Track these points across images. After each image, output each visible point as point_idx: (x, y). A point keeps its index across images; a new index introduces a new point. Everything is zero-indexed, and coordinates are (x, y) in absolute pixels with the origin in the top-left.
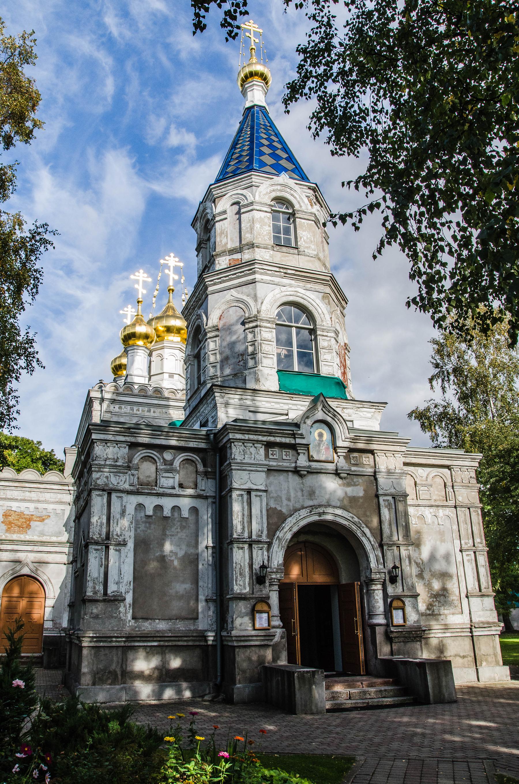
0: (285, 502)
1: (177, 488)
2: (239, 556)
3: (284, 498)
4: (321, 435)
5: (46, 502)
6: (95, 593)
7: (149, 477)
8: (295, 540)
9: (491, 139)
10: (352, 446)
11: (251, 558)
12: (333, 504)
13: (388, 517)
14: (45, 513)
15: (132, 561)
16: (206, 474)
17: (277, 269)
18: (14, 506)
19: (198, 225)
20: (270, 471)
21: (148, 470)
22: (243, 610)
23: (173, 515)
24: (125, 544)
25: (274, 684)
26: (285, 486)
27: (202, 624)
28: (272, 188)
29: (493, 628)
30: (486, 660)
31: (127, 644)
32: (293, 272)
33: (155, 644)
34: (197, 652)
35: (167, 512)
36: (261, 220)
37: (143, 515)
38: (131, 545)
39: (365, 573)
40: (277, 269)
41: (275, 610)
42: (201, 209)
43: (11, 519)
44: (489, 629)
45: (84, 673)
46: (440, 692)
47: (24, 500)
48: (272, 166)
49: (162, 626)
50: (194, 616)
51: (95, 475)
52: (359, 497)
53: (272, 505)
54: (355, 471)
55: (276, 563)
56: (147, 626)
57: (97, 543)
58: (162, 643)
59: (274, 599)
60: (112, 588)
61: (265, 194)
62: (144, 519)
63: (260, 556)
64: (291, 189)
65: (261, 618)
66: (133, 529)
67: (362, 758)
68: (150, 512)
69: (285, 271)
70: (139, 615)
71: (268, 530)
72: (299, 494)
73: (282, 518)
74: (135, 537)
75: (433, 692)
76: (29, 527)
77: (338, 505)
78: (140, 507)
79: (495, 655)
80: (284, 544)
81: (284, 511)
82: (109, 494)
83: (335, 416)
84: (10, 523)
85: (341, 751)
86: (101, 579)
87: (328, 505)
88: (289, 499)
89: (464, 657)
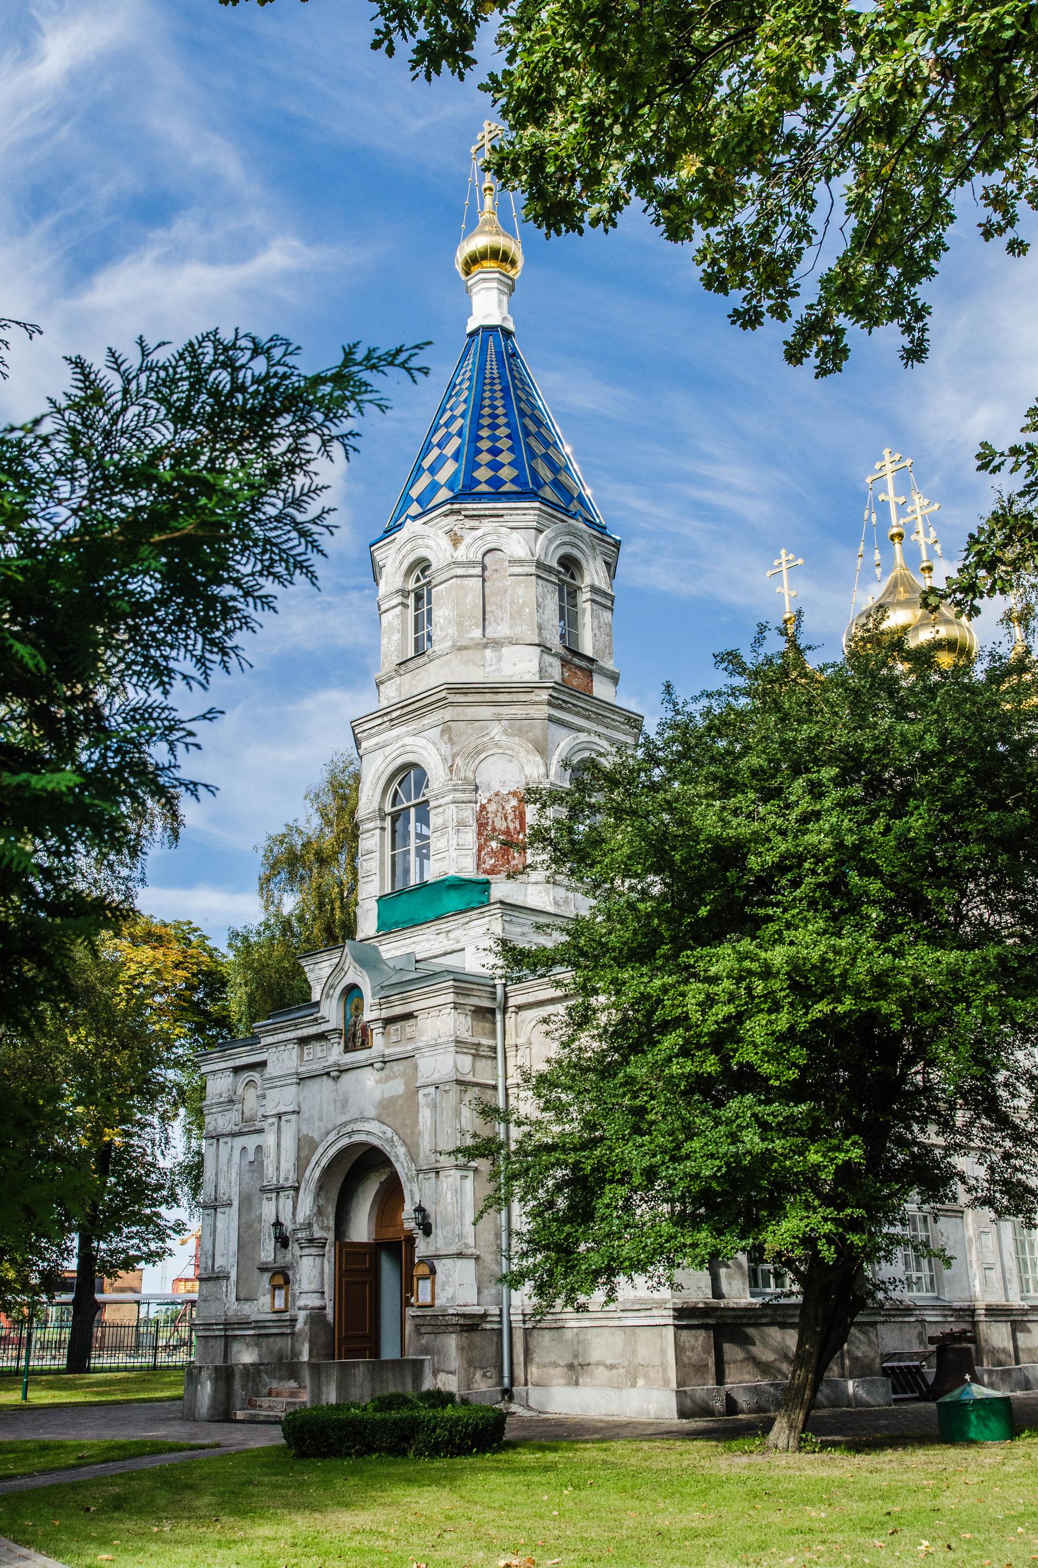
0: (317, 1124)
10: (385, 1014)
12: (367, 1115)
15: (710, 1283)
17: (379, 721)
20: (302, 1079)
24: (230, 1205)
29: (655, 1312)
30: (646, 1376)
32: (398, 713)
33: (252, 1332)
39: (980, 1252)
40: (379, 721)
44: (647, 1313)
53: (305, 1131)
54: (308, 1071)
64: (422, 537)
69: (389, 717)
72: (332, 1108)
73: (313, 1145)
79: (664, 1367)
83: (331, 987)
86: (210, 1253)
87: (363, 1119)
89: (612, 1367)
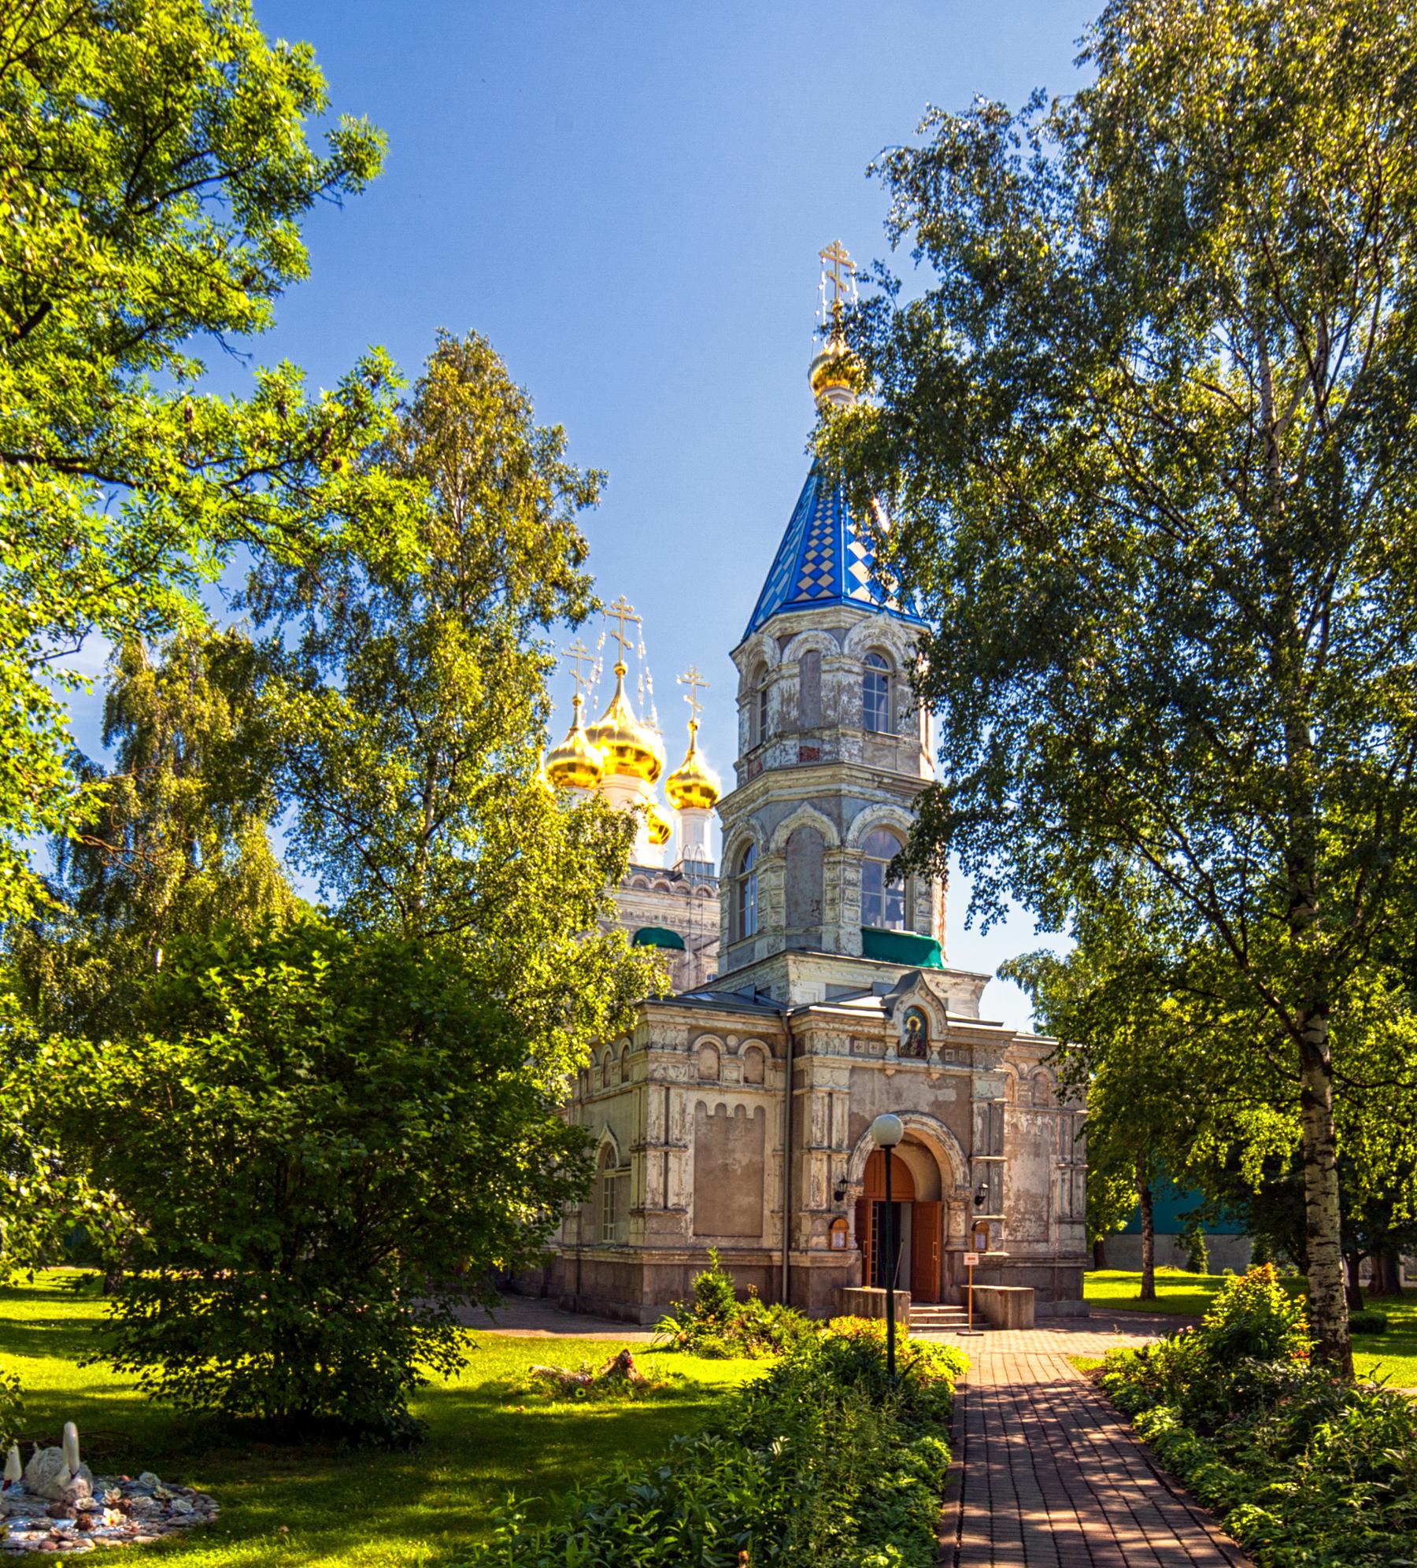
2: (817, 1169)
9: (1368, 724)
11: (830, 1171)
16: (775, 1067)
21: (708, 1059)
26: (869, 1086)
27: (768, 1242)
34: (762, 1272)
35: (730, 1112)
38: (691, 1151)
41: (852, 1230)
57: (655, 1146)
59: (851, 1218)
60: (672, 1200)
63: (839, 1166)
68: (712, 1112)
77: (927, 1110)
78: (700, 1104)
80: (865, 1155)
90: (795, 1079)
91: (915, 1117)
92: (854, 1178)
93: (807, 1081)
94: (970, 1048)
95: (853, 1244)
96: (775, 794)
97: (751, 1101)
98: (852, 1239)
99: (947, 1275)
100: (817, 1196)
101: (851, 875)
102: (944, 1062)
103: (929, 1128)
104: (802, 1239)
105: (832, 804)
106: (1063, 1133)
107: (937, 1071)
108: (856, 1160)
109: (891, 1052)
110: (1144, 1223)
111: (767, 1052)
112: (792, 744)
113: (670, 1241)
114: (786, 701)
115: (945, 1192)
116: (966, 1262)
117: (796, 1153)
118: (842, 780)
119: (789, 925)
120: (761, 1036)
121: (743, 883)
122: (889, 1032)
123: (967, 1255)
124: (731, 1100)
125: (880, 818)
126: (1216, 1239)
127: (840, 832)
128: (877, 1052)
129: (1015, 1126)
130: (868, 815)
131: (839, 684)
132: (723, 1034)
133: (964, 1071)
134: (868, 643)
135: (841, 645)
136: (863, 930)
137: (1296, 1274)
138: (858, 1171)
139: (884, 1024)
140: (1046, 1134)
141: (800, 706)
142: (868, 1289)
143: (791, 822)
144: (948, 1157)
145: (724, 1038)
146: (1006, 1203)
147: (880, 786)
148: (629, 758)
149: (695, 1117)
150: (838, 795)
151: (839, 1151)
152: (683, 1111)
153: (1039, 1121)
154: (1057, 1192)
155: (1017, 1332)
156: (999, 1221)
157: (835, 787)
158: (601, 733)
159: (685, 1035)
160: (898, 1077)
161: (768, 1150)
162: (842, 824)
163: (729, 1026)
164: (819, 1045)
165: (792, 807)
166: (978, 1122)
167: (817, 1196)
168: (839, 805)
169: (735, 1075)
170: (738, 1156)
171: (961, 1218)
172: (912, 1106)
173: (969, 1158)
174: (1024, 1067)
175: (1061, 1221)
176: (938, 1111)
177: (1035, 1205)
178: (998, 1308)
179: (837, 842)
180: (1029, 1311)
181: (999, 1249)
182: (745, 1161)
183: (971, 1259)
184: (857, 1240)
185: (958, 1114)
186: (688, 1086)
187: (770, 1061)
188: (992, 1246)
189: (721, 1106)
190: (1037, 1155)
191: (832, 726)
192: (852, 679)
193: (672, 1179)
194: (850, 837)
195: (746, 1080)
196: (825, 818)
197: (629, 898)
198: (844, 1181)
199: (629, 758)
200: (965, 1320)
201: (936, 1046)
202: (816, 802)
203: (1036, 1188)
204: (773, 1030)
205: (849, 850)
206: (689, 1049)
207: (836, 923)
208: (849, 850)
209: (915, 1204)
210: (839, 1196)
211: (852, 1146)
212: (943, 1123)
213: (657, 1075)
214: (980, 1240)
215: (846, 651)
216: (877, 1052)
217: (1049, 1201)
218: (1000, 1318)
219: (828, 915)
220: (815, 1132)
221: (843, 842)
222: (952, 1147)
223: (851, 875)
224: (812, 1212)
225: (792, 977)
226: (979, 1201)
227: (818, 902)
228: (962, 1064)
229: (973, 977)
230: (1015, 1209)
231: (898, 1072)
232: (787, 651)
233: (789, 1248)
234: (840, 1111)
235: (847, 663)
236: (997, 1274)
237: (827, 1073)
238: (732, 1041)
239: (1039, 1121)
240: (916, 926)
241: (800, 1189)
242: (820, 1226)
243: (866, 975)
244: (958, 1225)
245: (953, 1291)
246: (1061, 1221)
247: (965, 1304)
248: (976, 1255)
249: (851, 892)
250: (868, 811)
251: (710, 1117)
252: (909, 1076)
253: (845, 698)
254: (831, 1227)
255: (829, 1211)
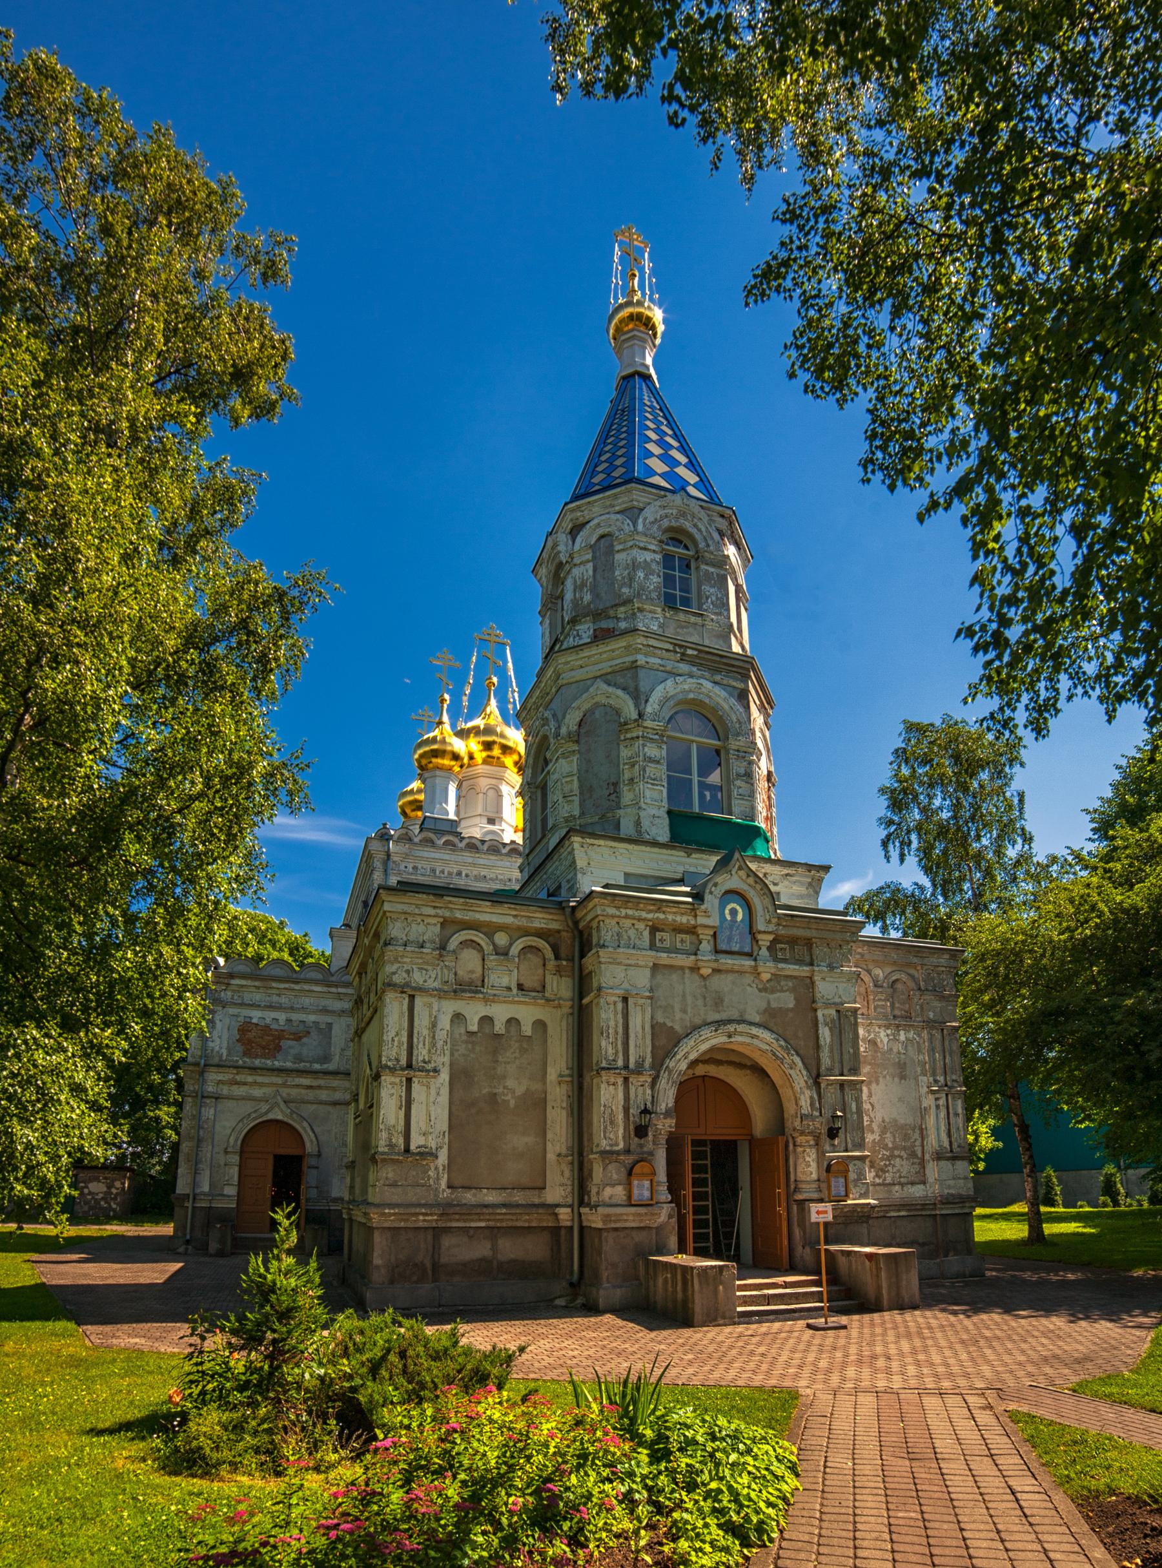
0: (678, 1015)
1: (515, 991)
2: (608, 1095)
3: (677, 1007)
4: (734, 912)
5: (303, 1009)
6: (391, 1145)
7: (472, 972)
8: (690, 1072)
12: (748, 1017)
13: (828, 1040)
14: (301, 1027)
16: (559, 971)
18: (256, 1015)
19: (543, 571)
21: (469, 963)
22: (615, 1176)
23: (508, 1030)
25: (660, 1281)
28: (662, 512)
31: (440, 1224)
35: (499, 1027)
36: (646, 565)
37: (463, 1031)
38: (444, 1076)
41: (662, 1176)
42: (550, 544)
43: (250, 1035)
45: (377, 1267)
46: (898, 1294)
47: (271, 1007)
48: (663, 476)
49: (491, 1197)
50: (539, 1184)
51: (389, 969)
52: (788, 1010)
53: (660, 1018)
55: (663, 1106)
56: (469, 1197)
57: (392, 1070)
58: (491, 1224)
60: (416, 1141)
61: (652, 523)
62: (464, 1038)
63: (641, 1093)
65: (641, 1187)
66: (447, 1053)
67: (808, 1391)
68: (474, 1028)
70: (456, 1183)
71: (653, 1057)
72: (700, 1002)
74: (451, 1065)
75: (889, 1293)
76: (278, 1048)
77: (757, 1019)
78: (458, 1017)
81: (677, 1027)
82: (412, 997)
84: (250, 1042)
85: (773, 1382)
86: (401, 1127)
88: (684, 1011)
90: (583, 984)
91: (741, 1028)
92: (662, 1107)
93: (595, 985)
94: (809, 943)
95: (664, 1195)
96: (566, 677)
97: (528, 1013)
98: (664, 1188)
99: (797, 1232)
100: (610, 1133)
101: (652, 751)
102: (776, 960)
103: (760, 1043)
104: (594, 1190)
105: (628, 678)
106: (932, 1050)
107: (767, 969)
108: (663, 1083)
109: (706, 946)
110: (1024, 1159)
111: (549, 953)
112: (586, 630)
113: (411, 1196)
114: (579, 587)
115: (788, 1124)
116: (814, 1218)
117: (587, 1079)
118: (638, 651)
119: (582, 814)
120: (540, 934)
121: (544, 788)
122: (701, 920)
123: (814, 1207)
124: (501, 1013)
125: (683, 691)
126: (1065, 1175)
127: (637, 705)
128: (687, 946)
129: (873, 1043)
130: (669, 687)
131: (634, 561)
132: (490, 930)
133: (804, 971)
134: (666, 523)
135: (635, 524)
136: (669, 813)
137: (1146, 1205)
138: (667, 1097)
139: (693, 911)
140: (912, 1052)
141: (594, 589)
142: (682, 1259)
143: (584, 703)
144: (789, 1078)
145: (490, 935)
146: (869, 1138)
147: (684, 658)
148: (496, 752)
149: (450, 1034)
150: (634, 667)
151: (639, 1071)
152: (434, 1025)
153: (902, 1036)
154: (931, 1121)
155: (896, 1316)
156: (862, 1159)
157: (631, 659)
158: (469, 731)
159: (438, 929)
160: (716, 978)
161: (552, 1075)
162: (638, 697)
163: (495, 919)
164: (607, 936)
165: (583, 686)
166: (825, 1034)
167: (610, 1133)
168: (635, 677)
169: (505, 981)
170: (510, 1083)
171: (811, 1156)
172: (737, 1014)
173: (816, 1080)
174: (879, 972)
175: (939, 1156)
176: (771, 1020)
177: (906, 1137)
178: (866, 1278)
179: (635, 716)
180: (911, 1282)
181: (864, 1195)
182: (520, 1090)
183: (821, 1213)
184: (670, 1190)
185: (799, 1022)
186: (441, 994)
187: (552, 964)
188: (854, 1191)
189: (487, 1020)
190: (903, 1077)
191: (628, 601)
192: (648, 556)
193: (420, 1114)
194: (649, 709)
195: (520, 987)
196: (619, 692)
197: (482, 861)
198: (645, 1111)
199: (496, 752)
200: (818, 1297)
201: (765, 940)
202: (607, 678)
203: (906, 1119)
204: (554, 926)
205: (648, 723)
206: (443, 947)
207: (636, 805)
208: (648, 723)
209: (752, 1141)
210: (641, 1131)
211: (658, 1065)
212: (780, 1036)
213: (397, 979)
214: (837, 1185)
215: (640, 527)
216: (687, 946)
217: (922, 1132)
218: (871, 1292)
219: (627, 797)
220: (605, 1047)
221: (641, 715)
222: (793, 1066)
223: (652, 751)
224: (604, 1153)
225: (580, 863)
226: (832, 1133)
227: (615, 784)
228: (800, 962)
229: (809, 867)
230: (881, 1144)
231: (716, 971)
232: (579, 539)
233: (581, 1203)
234: (639, 1021)
235: (642, 540)
236: (864, 1229)
237: (620, 972)
238: (501, 939)
239: (902, 1036)
240: (735, 809)
241: (590, 1124)
242: (615, 1172)
243: (676, 862)
244: (807, 1166)
245: (804, 1254)
246: (939, 1156)
247: (819, 1273)
248: (828, 1207)
249: (651, 770)
250: (670, 683)
251: (471, 1034)
252: (730, 977)
253: (641, 574)
254: (630, 1173)
255: (627, 1151)
